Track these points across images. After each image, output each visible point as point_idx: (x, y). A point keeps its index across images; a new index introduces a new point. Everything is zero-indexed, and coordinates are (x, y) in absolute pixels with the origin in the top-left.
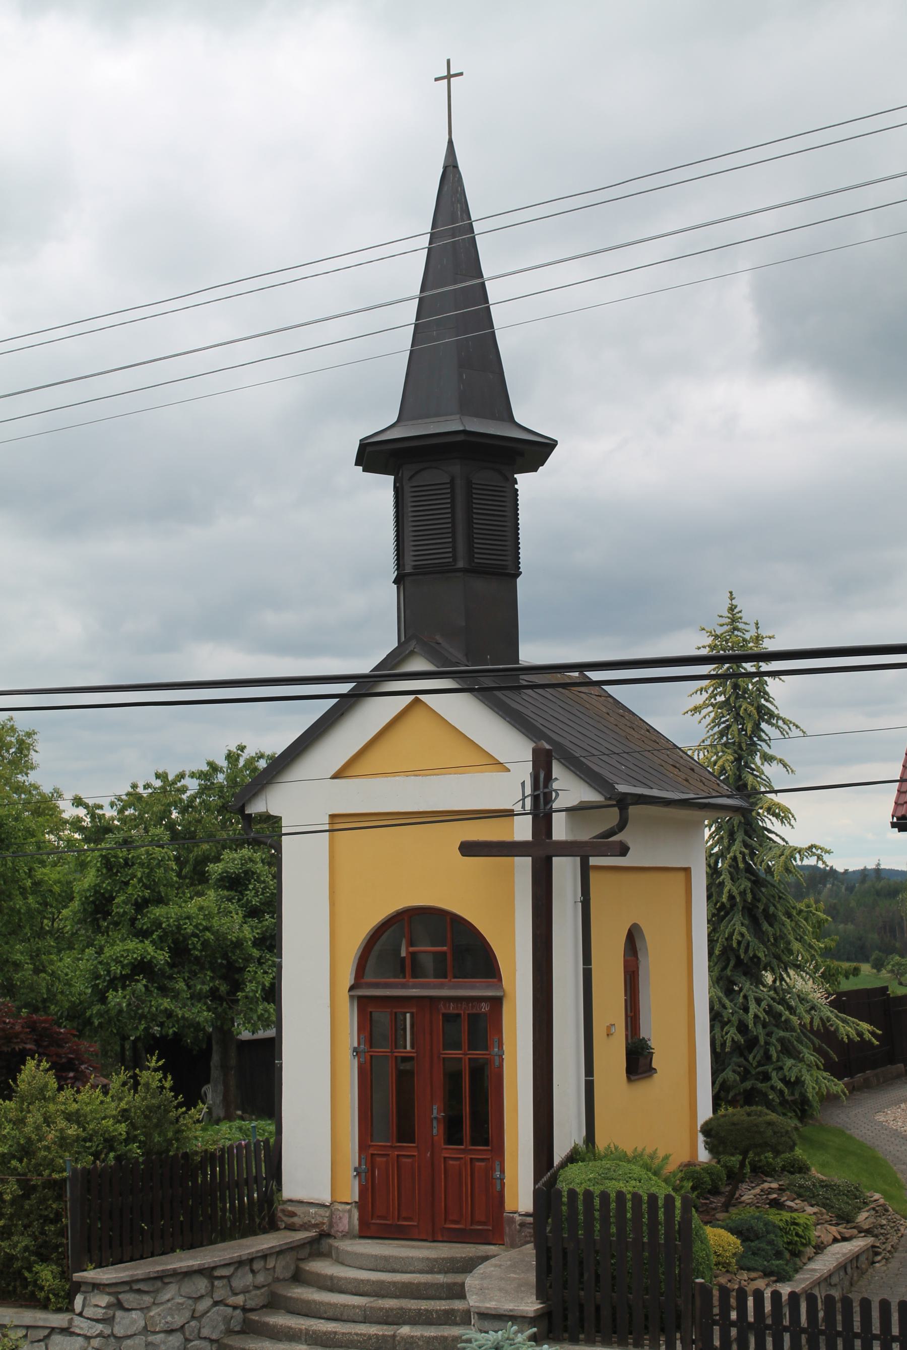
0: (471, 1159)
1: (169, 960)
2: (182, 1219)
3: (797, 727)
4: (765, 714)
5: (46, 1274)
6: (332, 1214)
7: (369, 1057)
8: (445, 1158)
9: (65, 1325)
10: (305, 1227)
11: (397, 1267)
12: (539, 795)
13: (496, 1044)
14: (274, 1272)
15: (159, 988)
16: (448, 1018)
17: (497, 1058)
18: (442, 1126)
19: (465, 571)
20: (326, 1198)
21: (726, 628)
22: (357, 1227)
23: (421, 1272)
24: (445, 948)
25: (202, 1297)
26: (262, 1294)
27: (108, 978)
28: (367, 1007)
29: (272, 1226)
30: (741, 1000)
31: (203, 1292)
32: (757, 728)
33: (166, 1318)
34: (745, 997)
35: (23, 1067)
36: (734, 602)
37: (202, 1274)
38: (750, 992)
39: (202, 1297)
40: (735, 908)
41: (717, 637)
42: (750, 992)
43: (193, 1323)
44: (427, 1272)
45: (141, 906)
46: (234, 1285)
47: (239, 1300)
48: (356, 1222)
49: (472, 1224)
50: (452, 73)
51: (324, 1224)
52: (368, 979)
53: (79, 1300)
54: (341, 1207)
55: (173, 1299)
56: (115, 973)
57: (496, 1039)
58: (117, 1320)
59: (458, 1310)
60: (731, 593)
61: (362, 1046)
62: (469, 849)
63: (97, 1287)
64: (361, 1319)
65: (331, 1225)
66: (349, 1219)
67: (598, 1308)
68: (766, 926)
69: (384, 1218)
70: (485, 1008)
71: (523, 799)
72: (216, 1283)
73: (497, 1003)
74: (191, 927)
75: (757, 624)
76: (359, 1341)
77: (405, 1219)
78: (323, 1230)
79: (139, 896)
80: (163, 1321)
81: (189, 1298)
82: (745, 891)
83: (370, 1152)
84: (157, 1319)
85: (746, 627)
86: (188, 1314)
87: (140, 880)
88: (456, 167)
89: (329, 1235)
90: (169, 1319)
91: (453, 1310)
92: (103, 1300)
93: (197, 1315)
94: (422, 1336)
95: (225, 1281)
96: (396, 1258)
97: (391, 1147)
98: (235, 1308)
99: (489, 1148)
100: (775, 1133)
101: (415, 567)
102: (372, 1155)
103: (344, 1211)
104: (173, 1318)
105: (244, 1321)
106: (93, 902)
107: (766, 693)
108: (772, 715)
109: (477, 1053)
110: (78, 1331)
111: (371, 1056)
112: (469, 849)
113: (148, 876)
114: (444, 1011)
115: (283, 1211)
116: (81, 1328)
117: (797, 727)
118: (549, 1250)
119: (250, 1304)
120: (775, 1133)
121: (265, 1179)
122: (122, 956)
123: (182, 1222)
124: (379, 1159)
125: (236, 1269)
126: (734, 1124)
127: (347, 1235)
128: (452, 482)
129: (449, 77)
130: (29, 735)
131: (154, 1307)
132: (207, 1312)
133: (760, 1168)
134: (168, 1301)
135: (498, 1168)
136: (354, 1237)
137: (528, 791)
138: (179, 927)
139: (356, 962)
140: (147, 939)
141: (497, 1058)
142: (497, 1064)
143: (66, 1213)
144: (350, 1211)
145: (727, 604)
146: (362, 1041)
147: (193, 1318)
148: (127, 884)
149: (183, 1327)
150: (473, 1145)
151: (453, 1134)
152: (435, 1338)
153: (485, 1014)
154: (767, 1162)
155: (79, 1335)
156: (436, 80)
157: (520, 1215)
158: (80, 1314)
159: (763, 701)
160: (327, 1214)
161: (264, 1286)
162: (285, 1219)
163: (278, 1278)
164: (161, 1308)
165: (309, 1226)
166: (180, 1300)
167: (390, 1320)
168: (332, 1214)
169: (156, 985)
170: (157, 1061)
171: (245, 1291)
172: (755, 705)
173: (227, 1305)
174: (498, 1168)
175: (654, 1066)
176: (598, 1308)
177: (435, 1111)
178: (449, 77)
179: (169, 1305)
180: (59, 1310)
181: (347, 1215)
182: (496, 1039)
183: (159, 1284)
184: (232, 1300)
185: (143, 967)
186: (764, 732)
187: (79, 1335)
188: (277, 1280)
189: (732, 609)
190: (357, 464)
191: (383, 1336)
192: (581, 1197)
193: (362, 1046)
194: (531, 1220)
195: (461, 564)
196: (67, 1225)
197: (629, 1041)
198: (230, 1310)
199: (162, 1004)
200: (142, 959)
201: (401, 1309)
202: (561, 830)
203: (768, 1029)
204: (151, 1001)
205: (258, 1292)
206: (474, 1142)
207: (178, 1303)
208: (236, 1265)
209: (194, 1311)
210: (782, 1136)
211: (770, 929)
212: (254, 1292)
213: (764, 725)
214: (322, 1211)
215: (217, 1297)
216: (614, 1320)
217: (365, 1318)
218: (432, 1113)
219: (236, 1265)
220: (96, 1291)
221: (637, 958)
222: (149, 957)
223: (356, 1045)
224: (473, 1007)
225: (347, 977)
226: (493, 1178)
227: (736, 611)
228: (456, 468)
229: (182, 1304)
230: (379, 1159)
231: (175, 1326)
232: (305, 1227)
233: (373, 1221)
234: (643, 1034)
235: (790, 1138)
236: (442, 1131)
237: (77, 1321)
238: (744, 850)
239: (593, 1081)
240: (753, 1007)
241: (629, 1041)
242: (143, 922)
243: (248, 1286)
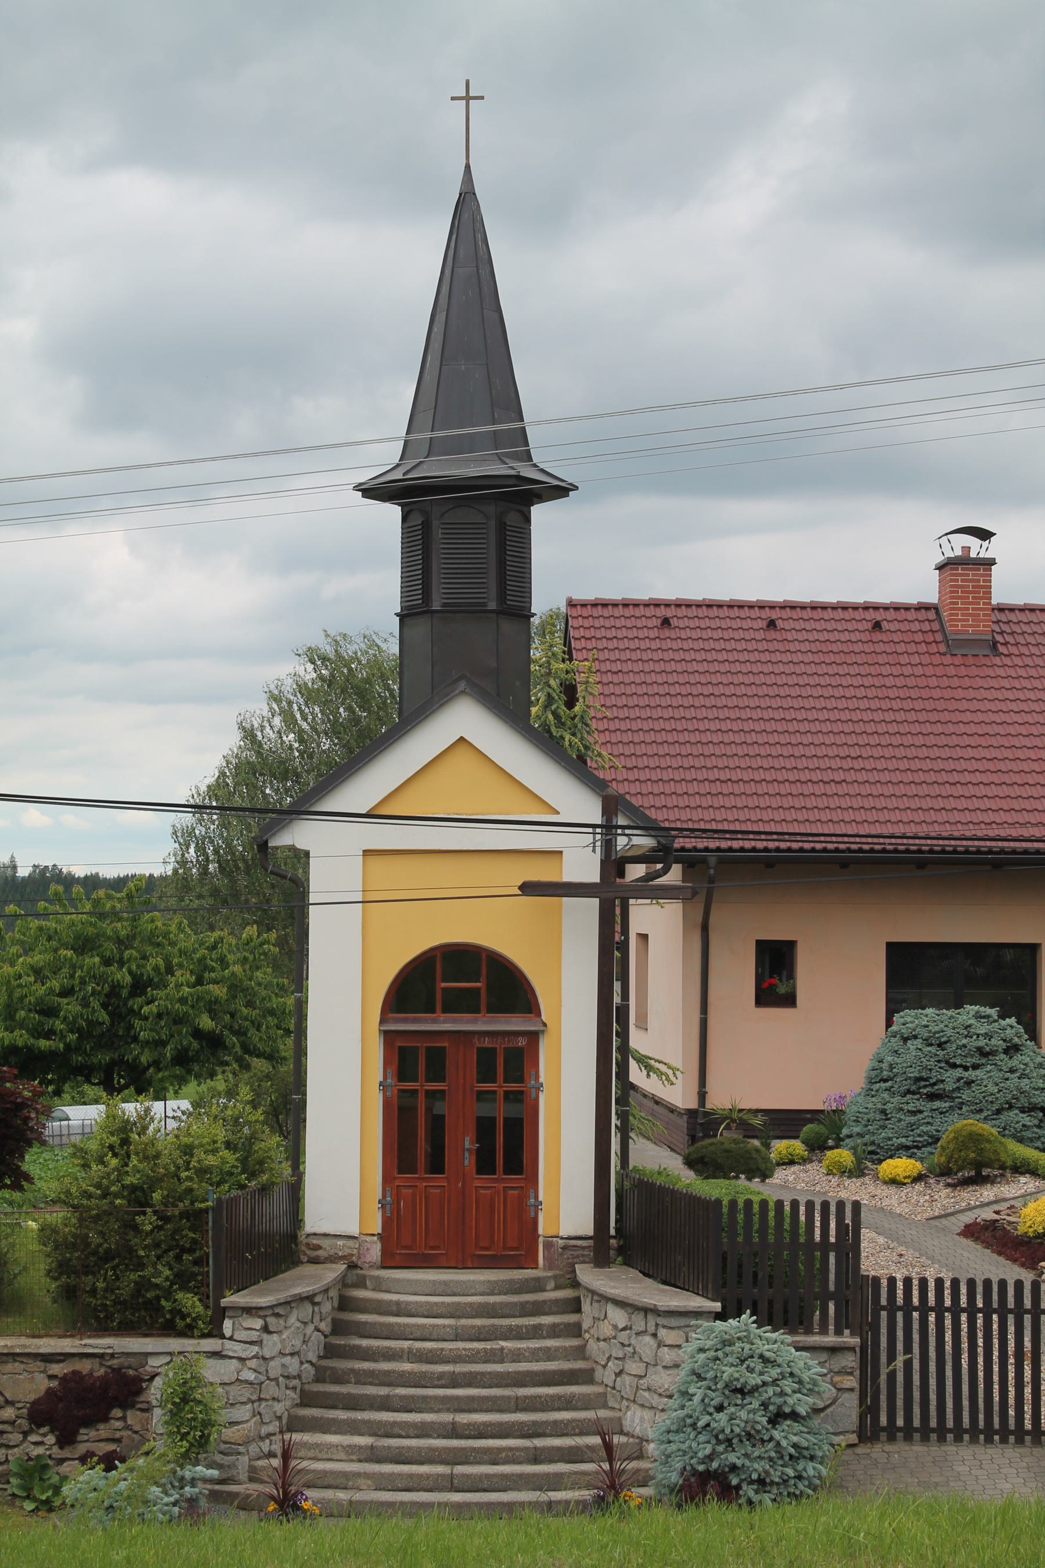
5: (190, 1301)
9: (218, 1349)
16: (482, 1051)
18: (474, 1158)
20: (355, 1231)
23: (482, 1294)
24: (479, 984)
44: (488, 1294)
51: (353, 1255)
53: (227, 1326)
54: (368, 1239)
58: (265, 1342)
59: (545, 1325)
62: (528, 889)
63: (249, 1311)
64: (451, 1337)
66: (375, 1252)
67: (771, 1303)
70: (522, 1042)
71: (594, 843)
76: (467, 1356)
77: (432, 1248)
91: (540, 1324)
92: (258, 1323)
94: (528, 1348)
96: (457, 1282)
101: (444, 605)
109: (514, 1086)
110: (231, 1354)
112: (528, 889)
116: (235, 1351)
127: (372, 1266)
129: (468, 98)
135: (532, 1195)
136: (377, 1268)
143: (207, 1242)
146: (389, 1075)
150: (505, 1174)
151: (485, 1164)
152: (540, 1349)
155: (231, 1358)
156: (482, 98)
157: (562, 1238)
158: (231, 1338)
162: (309, 1252)
167: (482, 1337)
174: (532, 1195)
176: (771, 1303)
180: (209, 1335)
187: (231, 1358)
191: (492, 1349)
193: (389, 1081)
194: (591, 1242)
196: (207, 1254)
201: (493, 1326)
206: (508, 1171)
209: (305, 1335)
214: (351, 1243)
217: (457, 1336)
218: (464, 1145)
220: (244, 1315)
224: (509, 1041)
232: (333, 1259)
236: (474, 1162)
237: (228, 1344)
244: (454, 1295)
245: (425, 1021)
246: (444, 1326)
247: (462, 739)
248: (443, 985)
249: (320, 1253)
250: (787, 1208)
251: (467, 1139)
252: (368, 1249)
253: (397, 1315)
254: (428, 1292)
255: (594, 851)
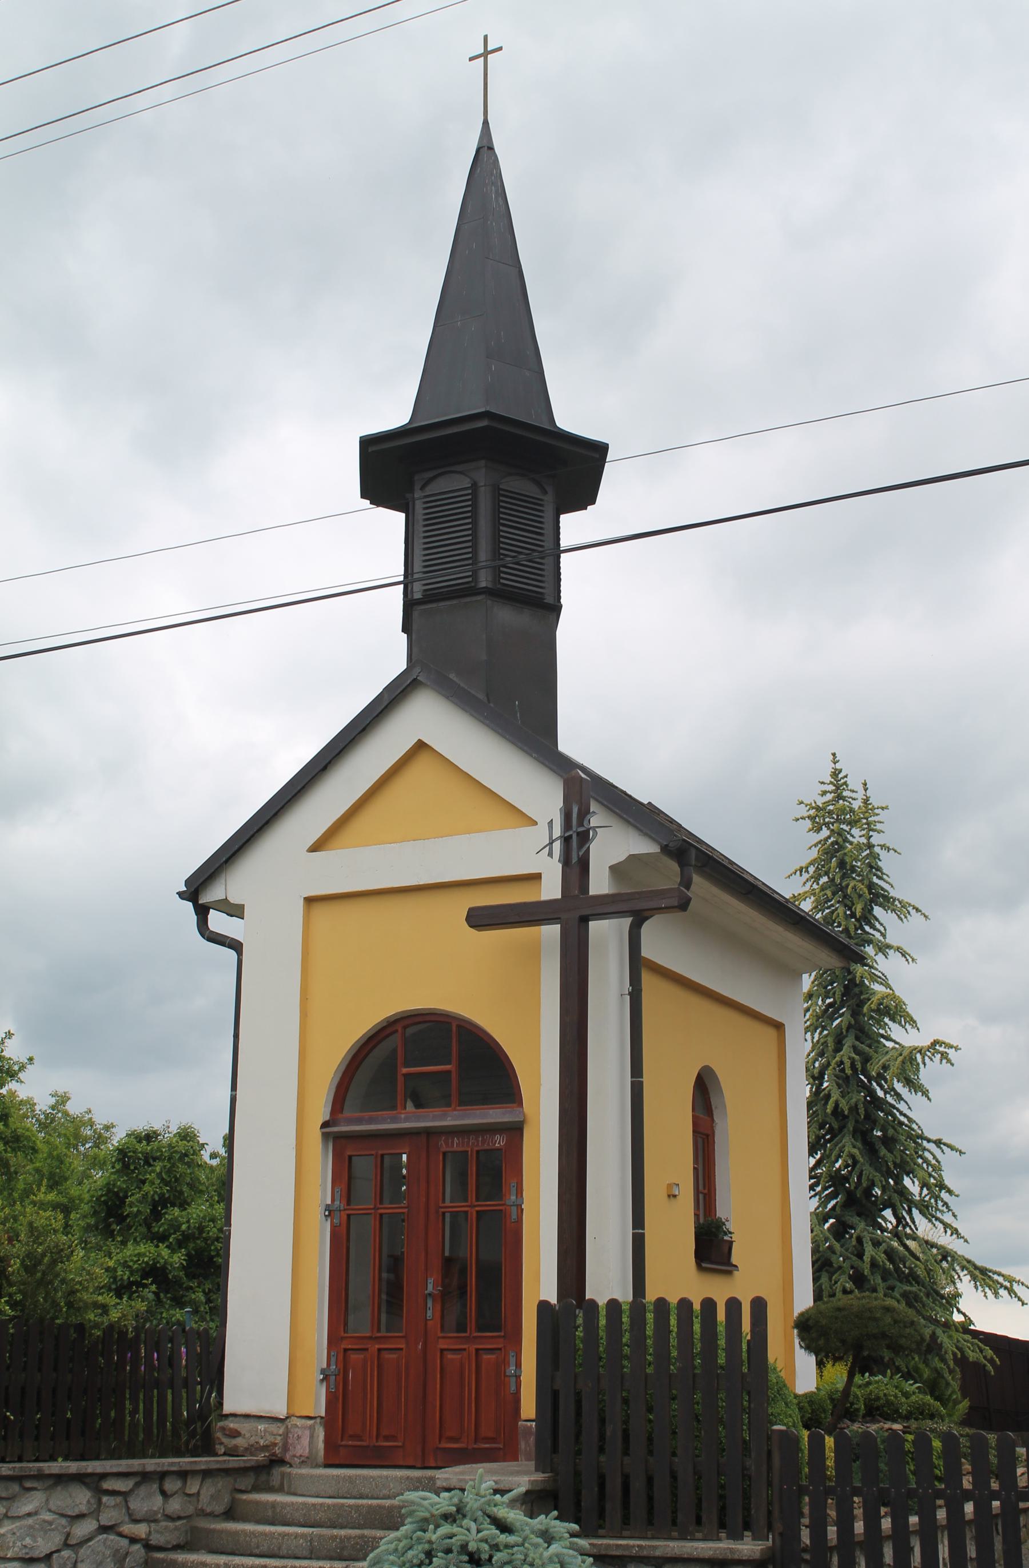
0: (477, 1350)
1: (184, 1263)
2: (69, 1415)
3: (918, 910)
4: (880, 897)
6: (287, 1432)
7: (345, 1217)
8: (442, 1350)
10: (252, 1449)
11: (366, 1491)
12: (571, 837)
13: (514, 1190)
14: (198, 1501)
15: (172, 1299)
17: (514, 1209)
19: (488, 592)
20: (281, 1411)
21: (829, 797)
22: (322, 1453)
25: (81, 1516)
26: (176, 1528)
27: (114, 1286)
28: (343, 1144)
29: (207, 1447)
30: (854, 1242)
31: (84, 1509)
32: (867, 917)
33: (24, 1539)
34: (859, 1240)
35: (60, 1459)
36: (838, 766)
37: (84, 1483)
38: (865, 1233)
39: (81, 1516)
40: (846, 1130)
41: (818, 809)
42: (865, 1233)
43: (66, 1553)
45: (158, 1207)
46: (132, 1506)
47: (141, 1530)
48: (321, 1446)
49: (475, 1443)
50: (489, 49)
51: (275, 1444)
52: (347, 1113)
55: (36, 1513)
56: (122, 1279)
57: (514, 1184)
60: (834, 755)
61: (337, 1203)
62: (481, 919)
64: (305, 1553)
65: (285, 1448)
66: (311, 1440)
68: (883, 1151)
69: (359, 1438)
70: (500, 1141)
71: (551, 843)
72: (105, 1499)
73: (515, 1131)
74: (215, 1230)
75: (865, 784)
77: (387, 1438)
78: (274, 1454)
79: (156, 1192)
80: (19, 1544)
81: (63, 1515)
82: (856, 1105)
83: (343, 1346)
84: (10, 1539)
85: (854, 795)
86: (57, 1539)
87: (159, 1175)
88: (491, 148)
89: (282, 1462)
90: (28, 1541)
93: (72, 1541)
95: (119, 1499)
97: (370, 1338)
98: (133, 1540)
99: (502, 1334)
100: (896, 1322)
102: (345, 1350)
103: (304, 1428)
104: (35, 1541)
105: (146, 1562)
106: (105, 1203)
107: (879, 869)
108: (887, 898)
109: (489, 1205)
111: (349, 1216)
113: (169, 1171)
114: (444, 1148)
115: (223, 1429)
117: (918, 910)
118: (555, 1394)
119: (156, 1540)
120: (896, 1322)
121: (200, 1383)
122: (132, 1260)
123: (69, 1420)
124: (354, 1357)
125: (137, 1485)
126: (839, 1309)
128: (474, 486)
129: (486, 54)
130: (107, 1128)
131: (6, 1522)
132: (89, 1539)
133: (878, 1408)
134: (29, 1515)
135: (513, 1360)
137: (557, 832)
138: (201, 1229)
139: (334, 1090)
140: (163, 1243)
141: (514, 1209)
142: (514, 1217)
144: (312, 1428)
145: (829, 768)
146: (337, 1196)
147: (66, 1545)
148: (143, 1182)
149: (48, 1557)
153: (499, 1149)
154: (887, 1401)
156: (471, 59)
159: (875, 880)
160: (281, 1431)
161: (179, 1518)
162: (225, 1440)
163: (202, 1510)
164: (18, 1524)
165: (256, 1449)
166: (48, 1517)
167: (345, 1553)
168: (287, 1432)
169: (169, 1295)
170: (195, 1428)
171: (150, 1519)
172: (866, 882)
173: (121, 1535)
174: (513, 1360)
175: (734, 1260)
177: (430, 1287)
178: (486, 54)
179: (30, 1521)
181: (307, 1433)
182: (514, 1184)
183: (15, 1488)
184: (128, 1528)
185: (155, 1272)
186: (877, 920)
188: (203, 1514)
189: (836, 773)
190: (362, 497)
192: (603, 1312)
193: (337, 1203)
195: (484, 581)
197: (702, 1221)
198: (125, 1542)
199: (174, 1315)
200: (155, 1264)
202: (600, 884)
203: (890, 1282)
204: (162, 1313)
205: (171, 1525)
207: (45, 1521)
208: (138, 1479)
209: (68, 1535)
210: (905, 1327)
211: (889, 1155)
212: (164, 1524)
213: (877, 911)
214: (273, 1427)
215: (106, 1519)
216: (650, 1499)
217: (311, 1553)
219: (138, 1479)
221: (713, 1120)
222: (162, 1261)
223: (329, 1202)
225: (320, 1110)
226: (505, 1376)
227: (840, 776)
228: (481, 474)
229: (50, 1523)
230: (354, 1357)
231: (36, 1554)
233: (343, 1443)
234: (721, 1213)
235: (916, 1330)
238: (854, 1055)
239: (643, 1234)
240: (869, 1250)
241: (702, 1221)
242: (159, 1228)
243: (156, 1513)
244: (361, 1497)
245: (383, 1121)
246: (297, 1536)
247: (421, 746)
248: (405, 1070)
249: (239, 1441)
250: (721, 1316)
251: (431, 1281)
252: (299, 1437)
253: (273, 1524)
254: (330, 1493)
255: (550, 854)
